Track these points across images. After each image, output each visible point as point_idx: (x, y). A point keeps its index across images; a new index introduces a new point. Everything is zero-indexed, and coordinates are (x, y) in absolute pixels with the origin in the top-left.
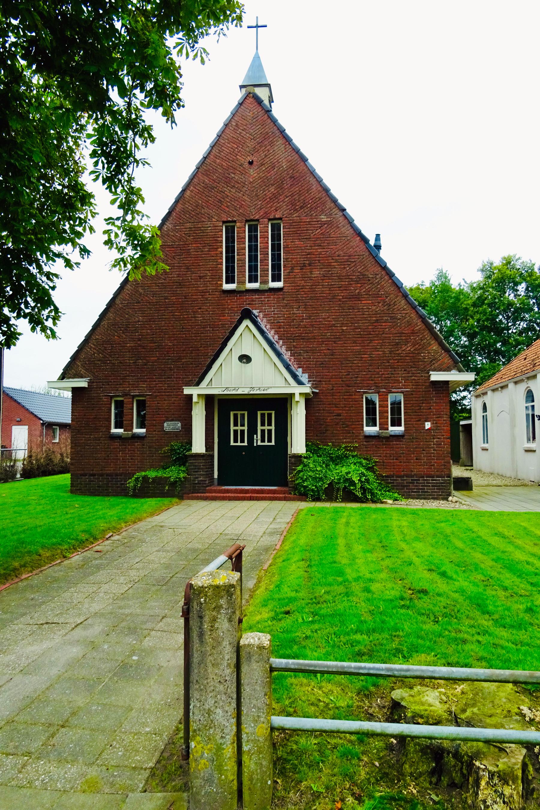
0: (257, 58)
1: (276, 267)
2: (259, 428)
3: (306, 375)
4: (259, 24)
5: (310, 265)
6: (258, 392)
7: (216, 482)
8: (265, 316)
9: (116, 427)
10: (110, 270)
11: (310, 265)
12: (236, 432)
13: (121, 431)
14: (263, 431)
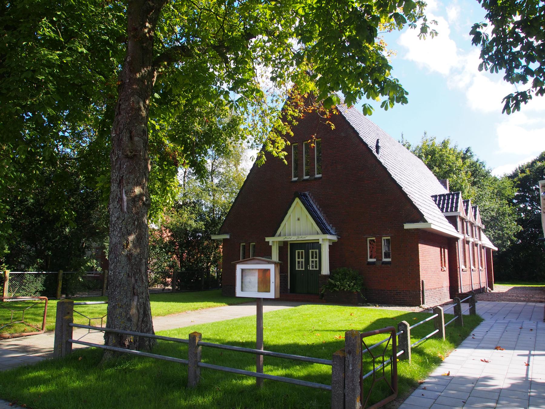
2: (311, 259)
3: (334, 228)
12: (299, 262)
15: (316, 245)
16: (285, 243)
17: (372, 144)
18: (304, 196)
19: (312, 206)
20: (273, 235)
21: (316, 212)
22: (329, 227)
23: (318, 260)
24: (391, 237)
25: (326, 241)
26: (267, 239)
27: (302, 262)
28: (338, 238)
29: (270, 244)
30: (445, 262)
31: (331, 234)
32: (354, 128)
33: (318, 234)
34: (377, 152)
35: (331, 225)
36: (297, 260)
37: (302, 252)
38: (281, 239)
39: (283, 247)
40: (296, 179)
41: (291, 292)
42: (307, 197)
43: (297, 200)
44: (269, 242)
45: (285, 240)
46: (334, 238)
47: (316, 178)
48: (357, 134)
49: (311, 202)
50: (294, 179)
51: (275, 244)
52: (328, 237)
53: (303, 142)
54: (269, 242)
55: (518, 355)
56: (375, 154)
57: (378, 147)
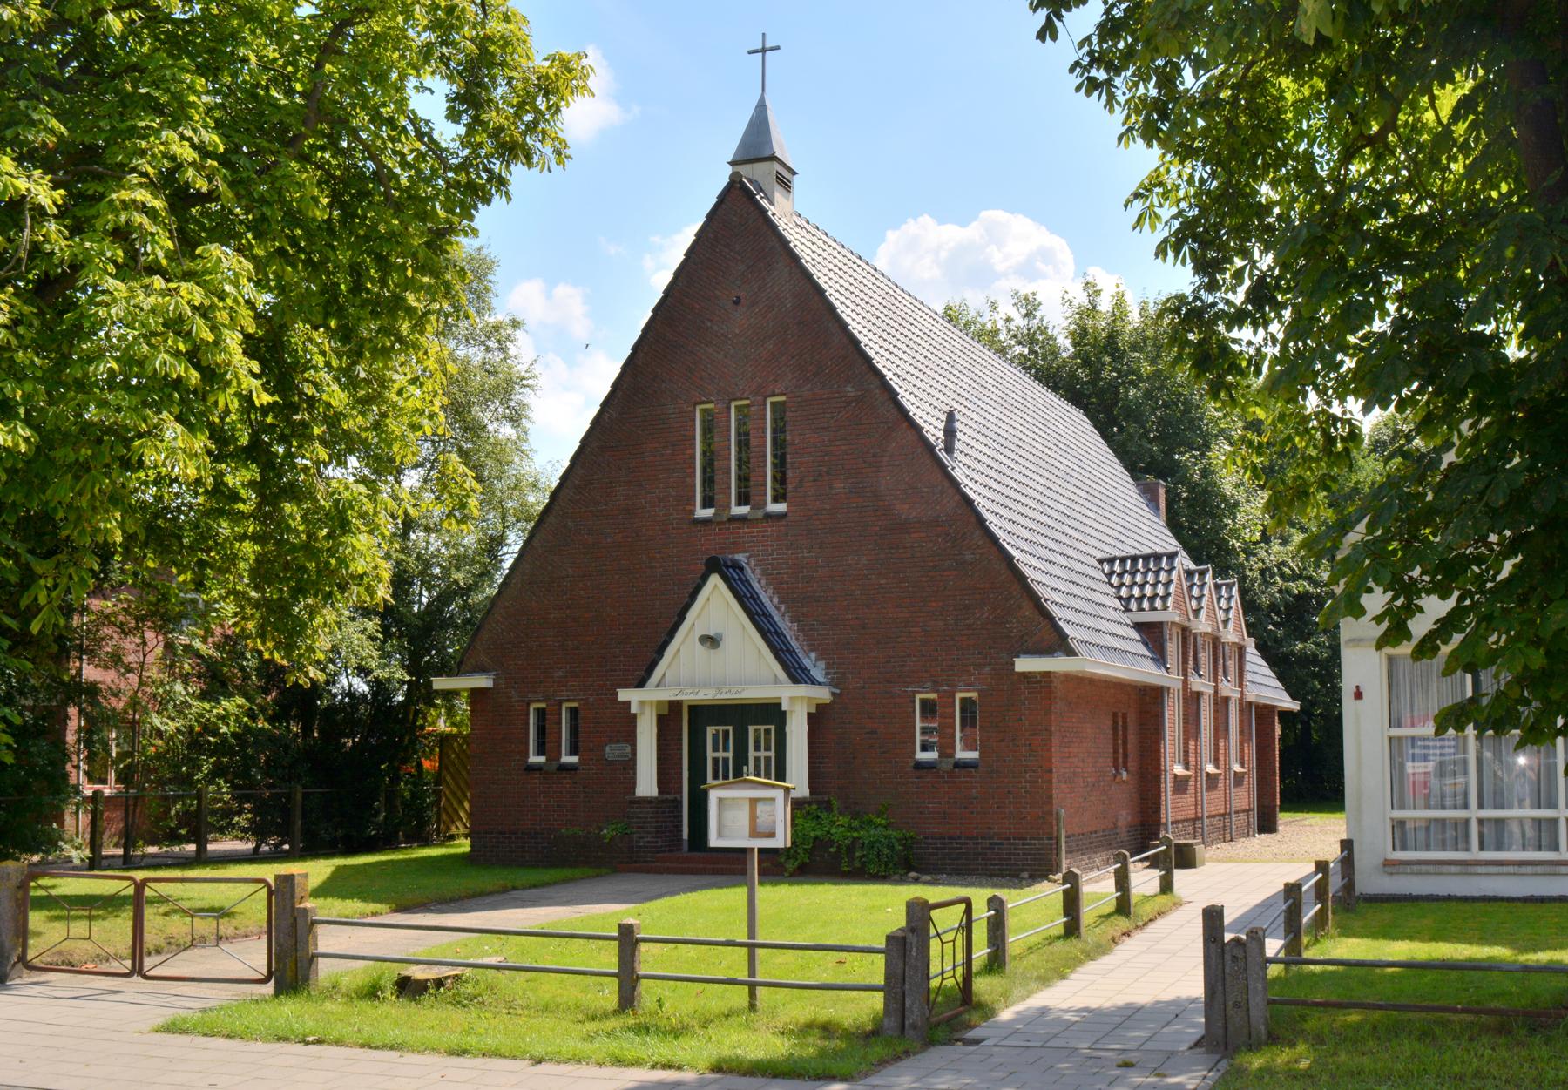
0: (761, 108)
1: (780, 479)
2: (752, 754)
3: (822, 664)
4: (768, 46)
5: (828, 473)
6: (728, 696)
7: (685, 846)
8: (759, 563)
9: (739, 504)
10: (509, 198)
11: (828, 473)
12: (716, 760)
13: (542, 759)
14: (757, 760)
15: (772, 713)
16: (675, 706)
17: (934, 431)
18: (734, 568)
19: (756, 599)
20: (641, 684)
21: (768, 617)
22: (807, 662)
23: (772, 754)
24: (980, 691)
25: (798, 701)
26: (624, 695)
27: (726, 760)
28: (833, 694)
29: (633, 710)
30: (1125, 728)
31: (813, 682)
32: (883, 376)
33: (777, 681)
34: (949, 449)
35: (813, 655)
36: (710, 754)
37: (726, 733)
38: (667, 695)
39: (669, 716)
40: (708, 513)
41: (691, 849)
42: (742, 569)
43: (715, 580)
44: (628, 703)
45: (679, 698)
46: (823, 694)
47: (769, 516)
48: (892, 395)
49: (756, 585)
50: (703, 513)
51: (648, 711)
52: (802, 690)
53: (731, 400)
54: (628, 703)
55: (171, 1028)
56: (943, 456)
57: (950, 432)
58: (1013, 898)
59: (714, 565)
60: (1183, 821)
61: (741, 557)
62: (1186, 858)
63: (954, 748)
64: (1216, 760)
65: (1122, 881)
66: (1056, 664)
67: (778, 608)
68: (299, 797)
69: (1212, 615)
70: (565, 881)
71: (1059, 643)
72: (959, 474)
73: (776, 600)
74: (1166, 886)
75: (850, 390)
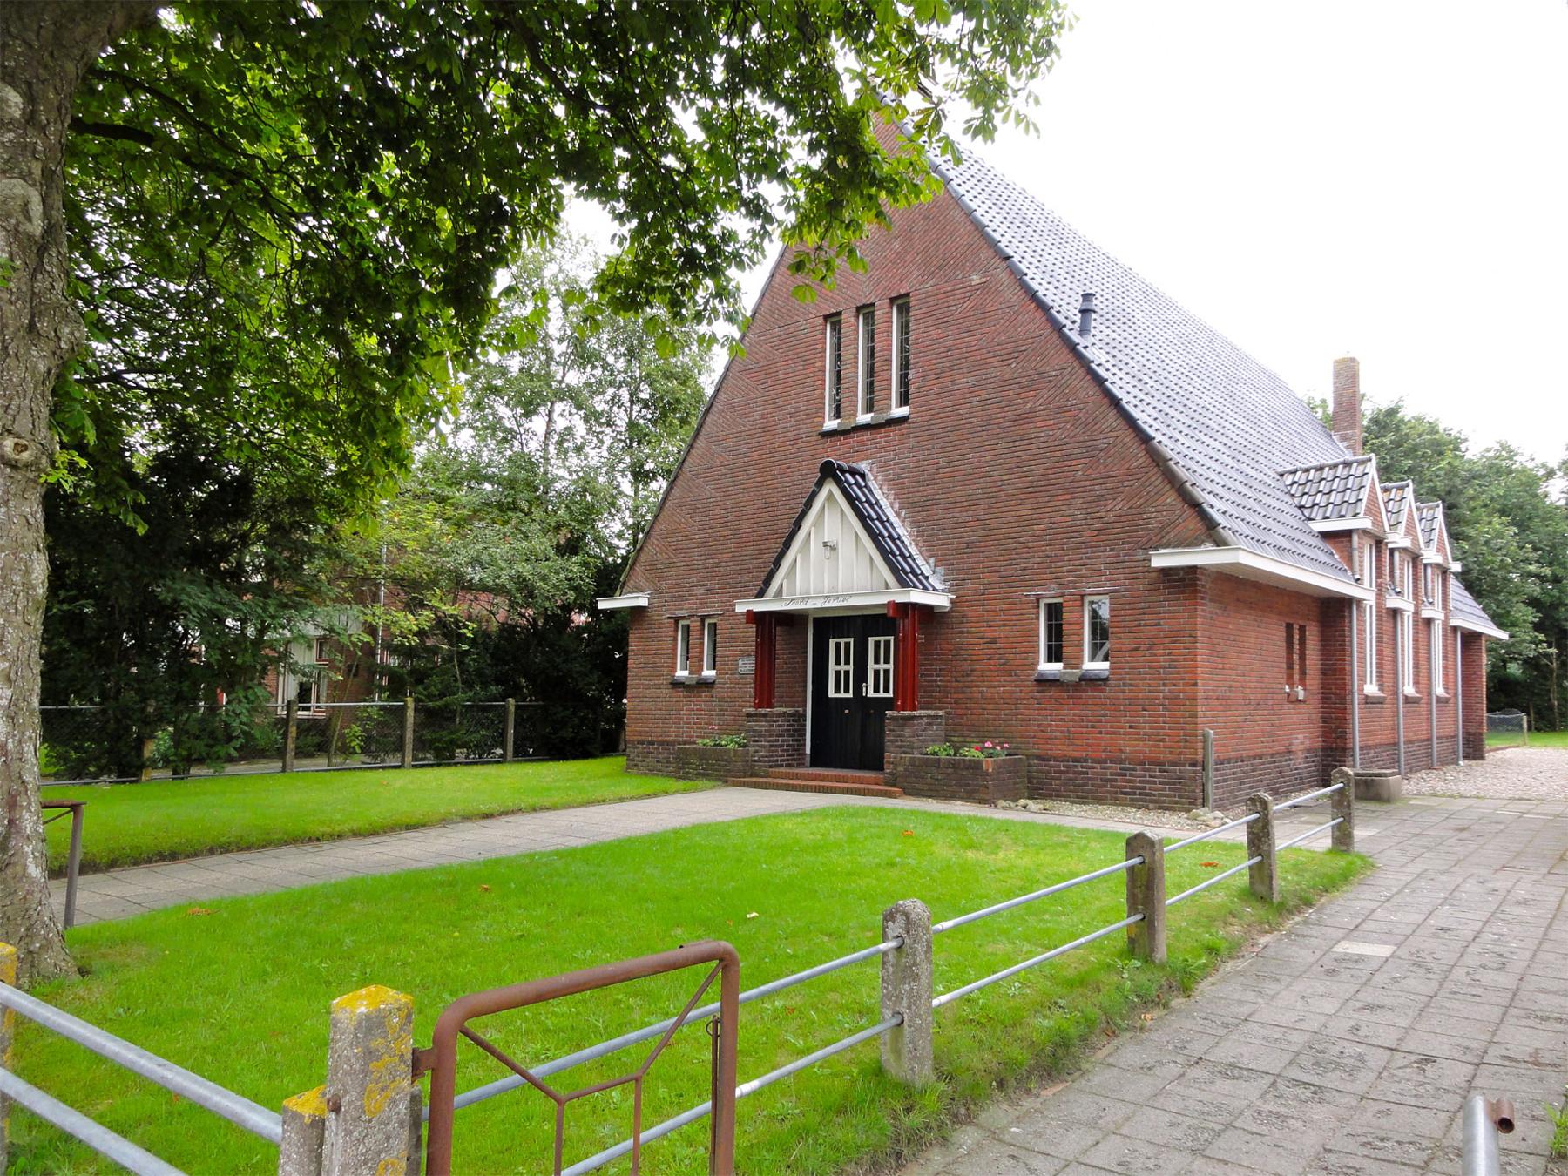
3: (941, 570)
12: (837, 673)
34: (1083, 331)
35: (932, 560)
58: (1170, 830)
59: (829, 471)
60: (1376, 746)
61: (864, 466)
62: (1371, 790)
63: (1081, 657)
64: (1416, 683)
65: (1259, 837)
66: (1204, 557)
67: (898, 514)
68: (512, 709)
69: (1410, 530)
70: (685, 791)
71: (1210, 531)
72: (1095, 354)
73: (897, 506)
74: (1343, 839)
75: (976, 279)
